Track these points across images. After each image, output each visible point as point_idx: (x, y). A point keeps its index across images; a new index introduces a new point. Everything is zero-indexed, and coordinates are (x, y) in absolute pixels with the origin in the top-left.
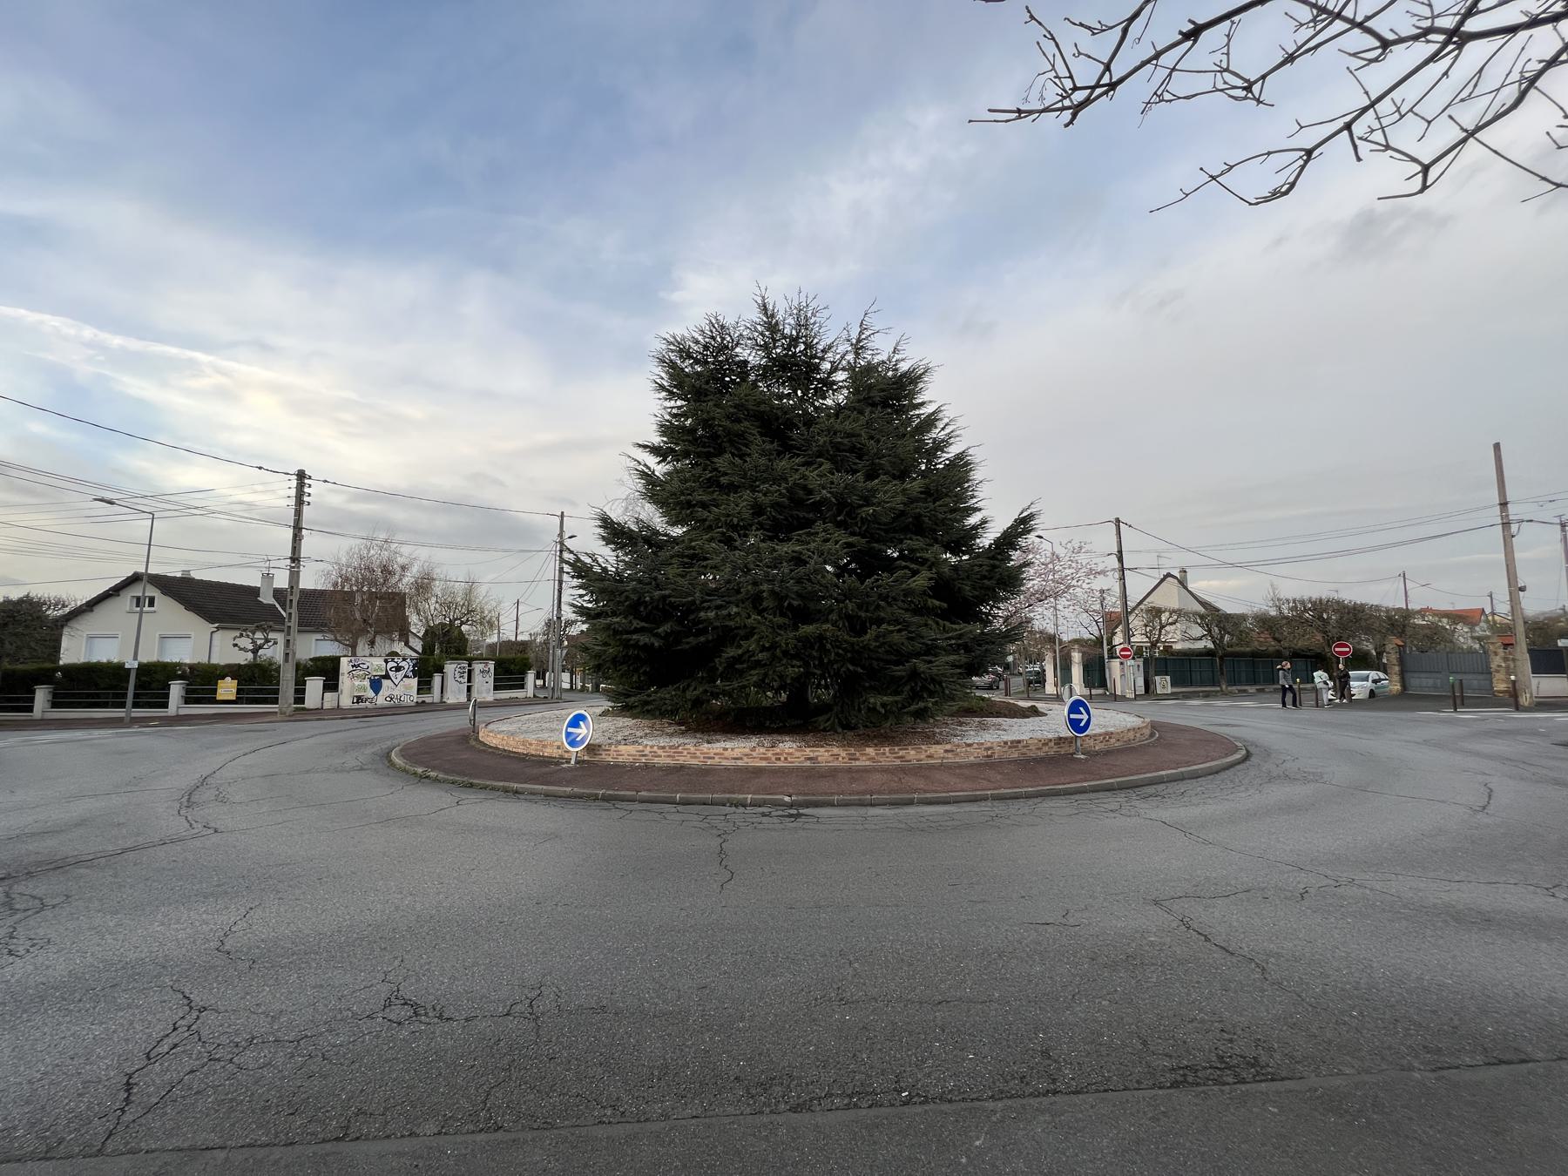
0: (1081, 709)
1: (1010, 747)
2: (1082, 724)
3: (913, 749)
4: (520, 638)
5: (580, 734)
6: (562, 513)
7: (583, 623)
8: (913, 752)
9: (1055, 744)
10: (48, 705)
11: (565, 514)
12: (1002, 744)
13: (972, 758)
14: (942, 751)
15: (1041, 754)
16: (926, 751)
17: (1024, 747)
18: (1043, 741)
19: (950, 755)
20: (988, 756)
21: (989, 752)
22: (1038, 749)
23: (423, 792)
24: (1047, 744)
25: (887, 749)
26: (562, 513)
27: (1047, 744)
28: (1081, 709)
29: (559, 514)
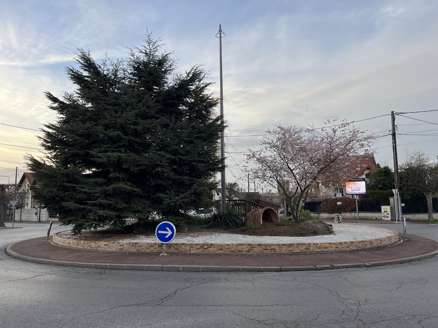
0: (168, 228)
1: (132, 246)
2: (167, 237)
3: (94, 242)
4: (250, 191)
5: (167, 234)
6: (393, 112)
7: (212, 182)
8: (93, 244)
9: (158, 247)
10: (49, 217)
11: (395, 113)
12: (128, 244)
13: (114, 249)
14: (103, 245)
15: (148, 251)
16: (98, 244)
17: (139, 246)
18: (150, 245)
19: (106, 247)
20: (121, 249)
21: (122, 247)
22: (147, 248)
23: (371, 271)
24: (153, 246)
25: (86, 242)
26: (393, 112)
27: (153, 246)
28: (168, 228)
29: (390, 113)
